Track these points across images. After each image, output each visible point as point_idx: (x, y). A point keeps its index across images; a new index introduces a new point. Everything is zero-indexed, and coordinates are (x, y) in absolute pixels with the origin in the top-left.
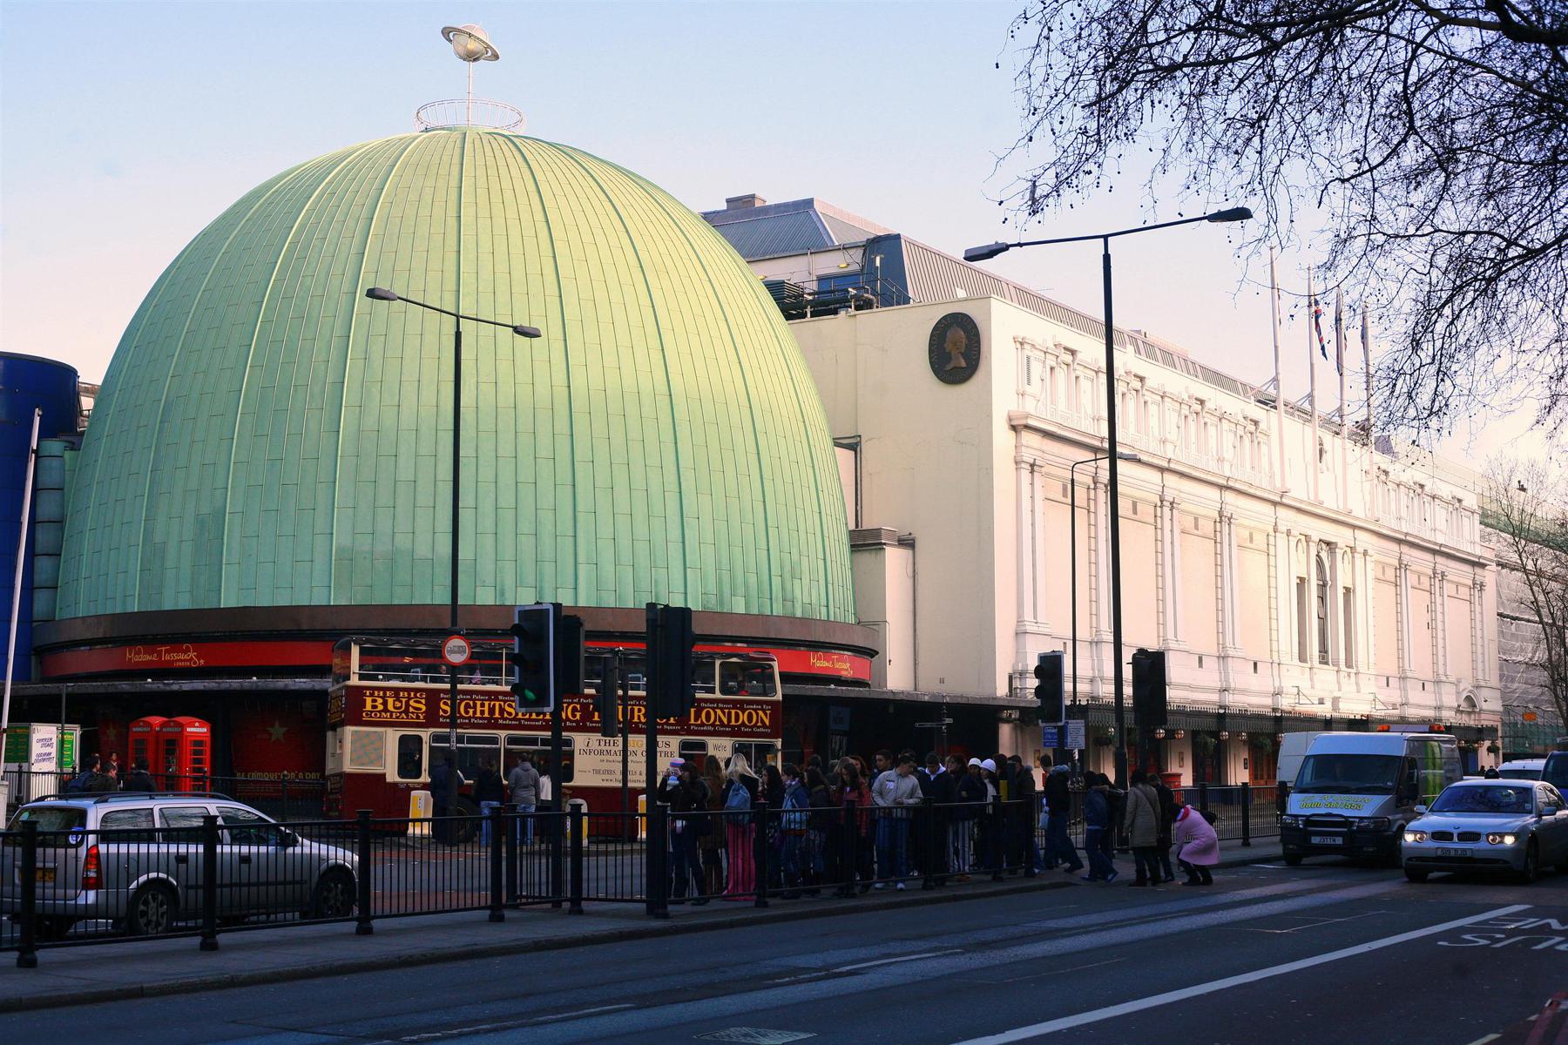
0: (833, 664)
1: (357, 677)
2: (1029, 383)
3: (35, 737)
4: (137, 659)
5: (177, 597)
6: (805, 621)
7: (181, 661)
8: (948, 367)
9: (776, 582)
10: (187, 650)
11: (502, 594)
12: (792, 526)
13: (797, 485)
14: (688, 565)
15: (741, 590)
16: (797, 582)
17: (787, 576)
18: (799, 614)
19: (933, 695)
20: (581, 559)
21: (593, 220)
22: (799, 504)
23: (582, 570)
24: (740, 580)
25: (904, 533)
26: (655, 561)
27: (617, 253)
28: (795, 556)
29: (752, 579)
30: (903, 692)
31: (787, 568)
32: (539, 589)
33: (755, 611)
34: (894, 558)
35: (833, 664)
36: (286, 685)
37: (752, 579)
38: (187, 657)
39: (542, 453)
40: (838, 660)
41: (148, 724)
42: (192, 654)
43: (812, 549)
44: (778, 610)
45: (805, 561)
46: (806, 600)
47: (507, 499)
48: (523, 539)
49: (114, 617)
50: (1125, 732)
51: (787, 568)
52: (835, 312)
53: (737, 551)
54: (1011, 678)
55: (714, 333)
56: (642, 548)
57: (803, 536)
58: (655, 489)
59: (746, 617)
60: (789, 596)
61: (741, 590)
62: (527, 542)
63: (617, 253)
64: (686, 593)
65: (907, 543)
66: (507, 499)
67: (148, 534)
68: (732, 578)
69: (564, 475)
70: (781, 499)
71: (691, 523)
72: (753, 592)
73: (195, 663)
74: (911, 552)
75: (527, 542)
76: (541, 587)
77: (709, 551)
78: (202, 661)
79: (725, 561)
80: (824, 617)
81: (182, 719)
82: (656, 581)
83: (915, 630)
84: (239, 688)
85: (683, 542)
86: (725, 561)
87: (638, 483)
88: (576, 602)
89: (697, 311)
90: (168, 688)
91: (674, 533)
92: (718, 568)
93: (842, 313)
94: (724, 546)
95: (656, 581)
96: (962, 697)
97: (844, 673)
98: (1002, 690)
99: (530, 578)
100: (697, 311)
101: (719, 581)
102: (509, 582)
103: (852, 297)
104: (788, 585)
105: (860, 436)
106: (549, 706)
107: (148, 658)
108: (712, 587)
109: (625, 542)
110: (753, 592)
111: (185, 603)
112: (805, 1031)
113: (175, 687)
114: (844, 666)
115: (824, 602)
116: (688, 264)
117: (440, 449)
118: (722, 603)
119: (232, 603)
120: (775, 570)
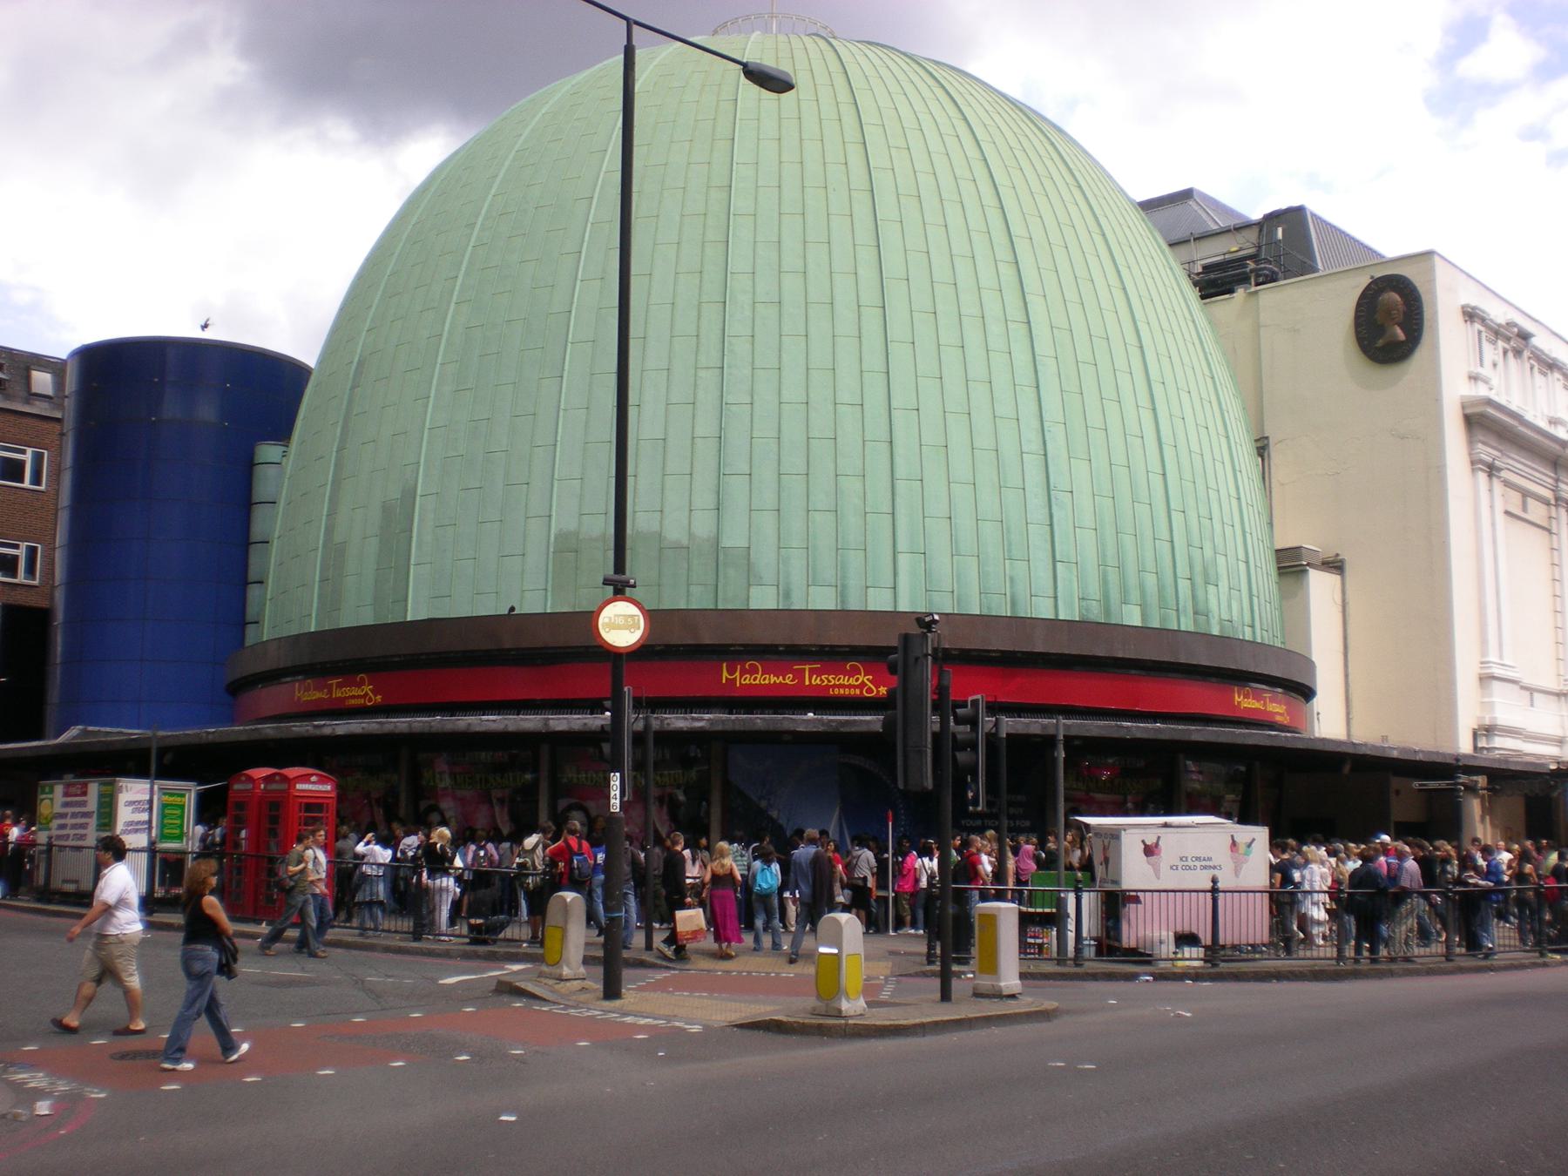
0: (1265, 704)
1: (640, 726)
2: (1482, 365)
3: (123, 798)
4: (748, 680)
5: (358, 612)
6: (1225, 642)
7: (354, 697)
8: (1380, 343)
9: (1184, 586)
10: (359, 685)
11: (787, 595)
12: (1203, 512)
13: (1208, 457)
14: (1058, 558)
15: (1135, 595)
16: (1211, 589)
17: (1199, 580)
18: (1215, 631)
19: (1404, 750)
20: (901, 546)
21: (918, 106)
22: (1212, 484)
23: (903, 560)
24: (1132, 581)
25: (1329, 554)
26: (1009, 551)
27: (951, 142)
28: (1208, 552)
29: (1151, 581)
30: (1365, 745)
31: (1198, 568)
32: (842, 593)
33: (1156, 624)
34: (1320, 584)
35: (1265, 704)
36: (585, 724)
37: (1151, 581)
38: (363, 692)
39: (844, 396)
40: (1272, 700)
41: (250, 779)
42: (367, 688)
43: (1230, 545)
44: (1187, 624)
45: (1221, 560)
46: (1225, 616)
47: (793, 462)
48: (818, 517)
49: (297, 638)
50: (69, 799)
51: (1198, 568)
52: (1231, 291)
53: (1128, 541)
54: (1475, 735)
55: (1087, 247)
56: (990, 531)
57: (1218, 527)
58: (1009, 449)
59: (1143, 632)
60: (1201, 606)
61: (1135, 595)
62: (823, 521)
63: (951, 142)
64: (1056, 598)
65: (1335, 565)
66: (793, 462)
67: (330, 530)
68: (1121, 567)
69: (878, 430)
70: (1187, 476)
71: (1061, 497)
72: (1153, 599)
73: (370, 700)
74: (1338, 577)
75: (823, 521)
76: (844, 586)
77: (1087, 539)
78: (379, 698)
79: (1112, 561)
80: (1248, 637)
81: (292, 772)
82: (1012, 579)
83: (1346, 676)
84: (581, 728)
85: (1051, 525)
86: (1111, 551)
87: (984, 440)
88: (895, 607)
89: (1063, 218)
90: (318, 732)
91: (1038, 512)
92: (1102, 564)
93: (1240, 293)
94: (1109, 533)
95: (1012, 579)
96: (1438, 753)
97: (1278, 718)
98: (1465, 746)
99: (828, 574)
100: (1063, 218)
101: (1104, 582)
102: (797, 578)
103: (1252, 271)
104: (1200, 593)
105: (1267, 438)
106: (25, 579)
107: (318, 695)
108: (1094, 590)
109: (965, 521)
110: (1153, 599)
111: (367, 618)
112: (1077, 820)
113: (327, 731)
114: (1276, 707)
115: (1247, 619)
116: (1049, 163)
117: (701, 395)
118: (1107, 611)
119: (422, 615)
120: (1182, 570)
